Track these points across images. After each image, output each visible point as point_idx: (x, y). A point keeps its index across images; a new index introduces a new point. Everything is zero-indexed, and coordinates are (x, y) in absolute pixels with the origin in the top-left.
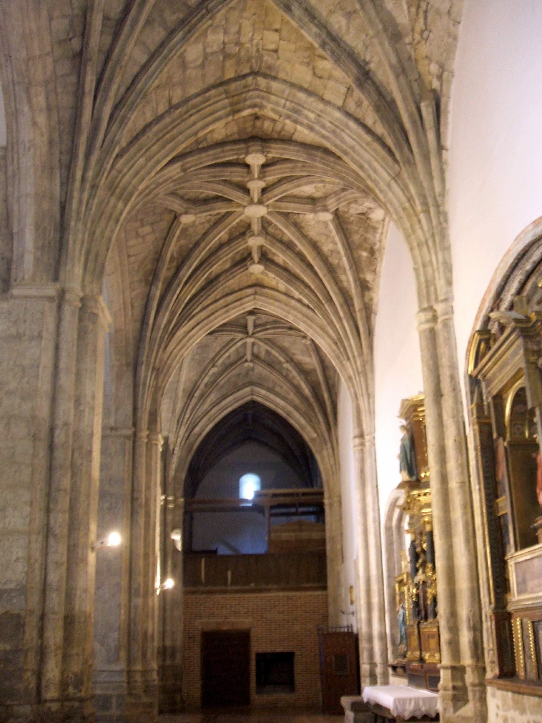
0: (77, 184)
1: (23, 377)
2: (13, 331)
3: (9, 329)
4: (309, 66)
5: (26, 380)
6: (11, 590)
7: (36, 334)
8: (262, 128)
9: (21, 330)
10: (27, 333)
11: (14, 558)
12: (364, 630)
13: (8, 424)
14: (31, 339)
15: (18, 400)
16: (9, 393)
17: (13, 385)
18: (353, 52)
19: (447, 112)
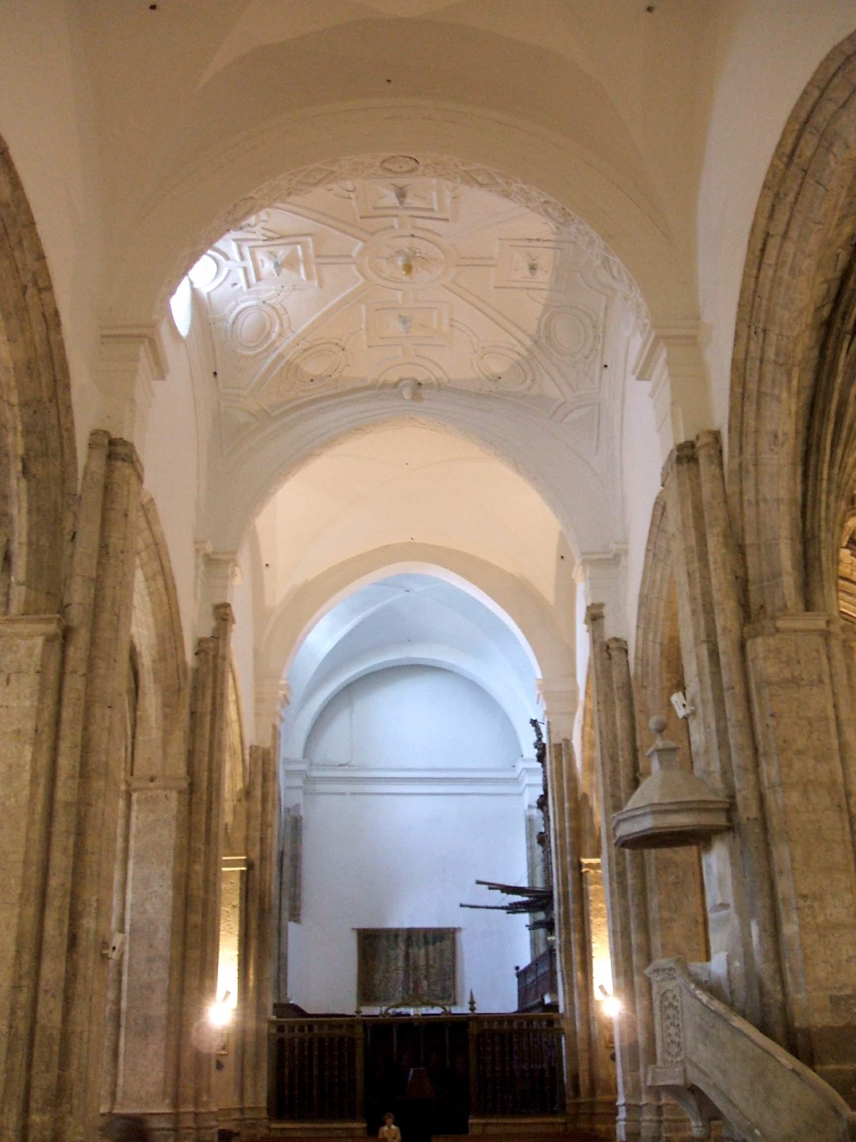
0: (824, 484)
1: (811, 732)
2: (787, 673)
3: (782, 672)
4: (356, 1012)
5: (815, 736)
6: (849, 997)
7: (815, 677)
8: (385, 1119)
9: (796, 673)
10: (805, 676)
11: (845, 957)
12: (624, 810)
13: (805, 791)
14: (812, 684)
15: (811, 763)
16: (799, 753)
17: (801, 743)
18: (300, 821)
19: (434, 660)
